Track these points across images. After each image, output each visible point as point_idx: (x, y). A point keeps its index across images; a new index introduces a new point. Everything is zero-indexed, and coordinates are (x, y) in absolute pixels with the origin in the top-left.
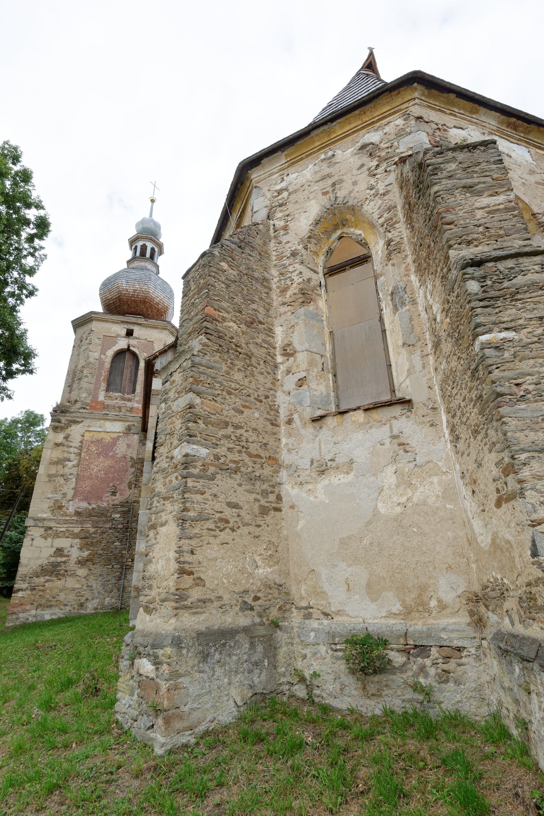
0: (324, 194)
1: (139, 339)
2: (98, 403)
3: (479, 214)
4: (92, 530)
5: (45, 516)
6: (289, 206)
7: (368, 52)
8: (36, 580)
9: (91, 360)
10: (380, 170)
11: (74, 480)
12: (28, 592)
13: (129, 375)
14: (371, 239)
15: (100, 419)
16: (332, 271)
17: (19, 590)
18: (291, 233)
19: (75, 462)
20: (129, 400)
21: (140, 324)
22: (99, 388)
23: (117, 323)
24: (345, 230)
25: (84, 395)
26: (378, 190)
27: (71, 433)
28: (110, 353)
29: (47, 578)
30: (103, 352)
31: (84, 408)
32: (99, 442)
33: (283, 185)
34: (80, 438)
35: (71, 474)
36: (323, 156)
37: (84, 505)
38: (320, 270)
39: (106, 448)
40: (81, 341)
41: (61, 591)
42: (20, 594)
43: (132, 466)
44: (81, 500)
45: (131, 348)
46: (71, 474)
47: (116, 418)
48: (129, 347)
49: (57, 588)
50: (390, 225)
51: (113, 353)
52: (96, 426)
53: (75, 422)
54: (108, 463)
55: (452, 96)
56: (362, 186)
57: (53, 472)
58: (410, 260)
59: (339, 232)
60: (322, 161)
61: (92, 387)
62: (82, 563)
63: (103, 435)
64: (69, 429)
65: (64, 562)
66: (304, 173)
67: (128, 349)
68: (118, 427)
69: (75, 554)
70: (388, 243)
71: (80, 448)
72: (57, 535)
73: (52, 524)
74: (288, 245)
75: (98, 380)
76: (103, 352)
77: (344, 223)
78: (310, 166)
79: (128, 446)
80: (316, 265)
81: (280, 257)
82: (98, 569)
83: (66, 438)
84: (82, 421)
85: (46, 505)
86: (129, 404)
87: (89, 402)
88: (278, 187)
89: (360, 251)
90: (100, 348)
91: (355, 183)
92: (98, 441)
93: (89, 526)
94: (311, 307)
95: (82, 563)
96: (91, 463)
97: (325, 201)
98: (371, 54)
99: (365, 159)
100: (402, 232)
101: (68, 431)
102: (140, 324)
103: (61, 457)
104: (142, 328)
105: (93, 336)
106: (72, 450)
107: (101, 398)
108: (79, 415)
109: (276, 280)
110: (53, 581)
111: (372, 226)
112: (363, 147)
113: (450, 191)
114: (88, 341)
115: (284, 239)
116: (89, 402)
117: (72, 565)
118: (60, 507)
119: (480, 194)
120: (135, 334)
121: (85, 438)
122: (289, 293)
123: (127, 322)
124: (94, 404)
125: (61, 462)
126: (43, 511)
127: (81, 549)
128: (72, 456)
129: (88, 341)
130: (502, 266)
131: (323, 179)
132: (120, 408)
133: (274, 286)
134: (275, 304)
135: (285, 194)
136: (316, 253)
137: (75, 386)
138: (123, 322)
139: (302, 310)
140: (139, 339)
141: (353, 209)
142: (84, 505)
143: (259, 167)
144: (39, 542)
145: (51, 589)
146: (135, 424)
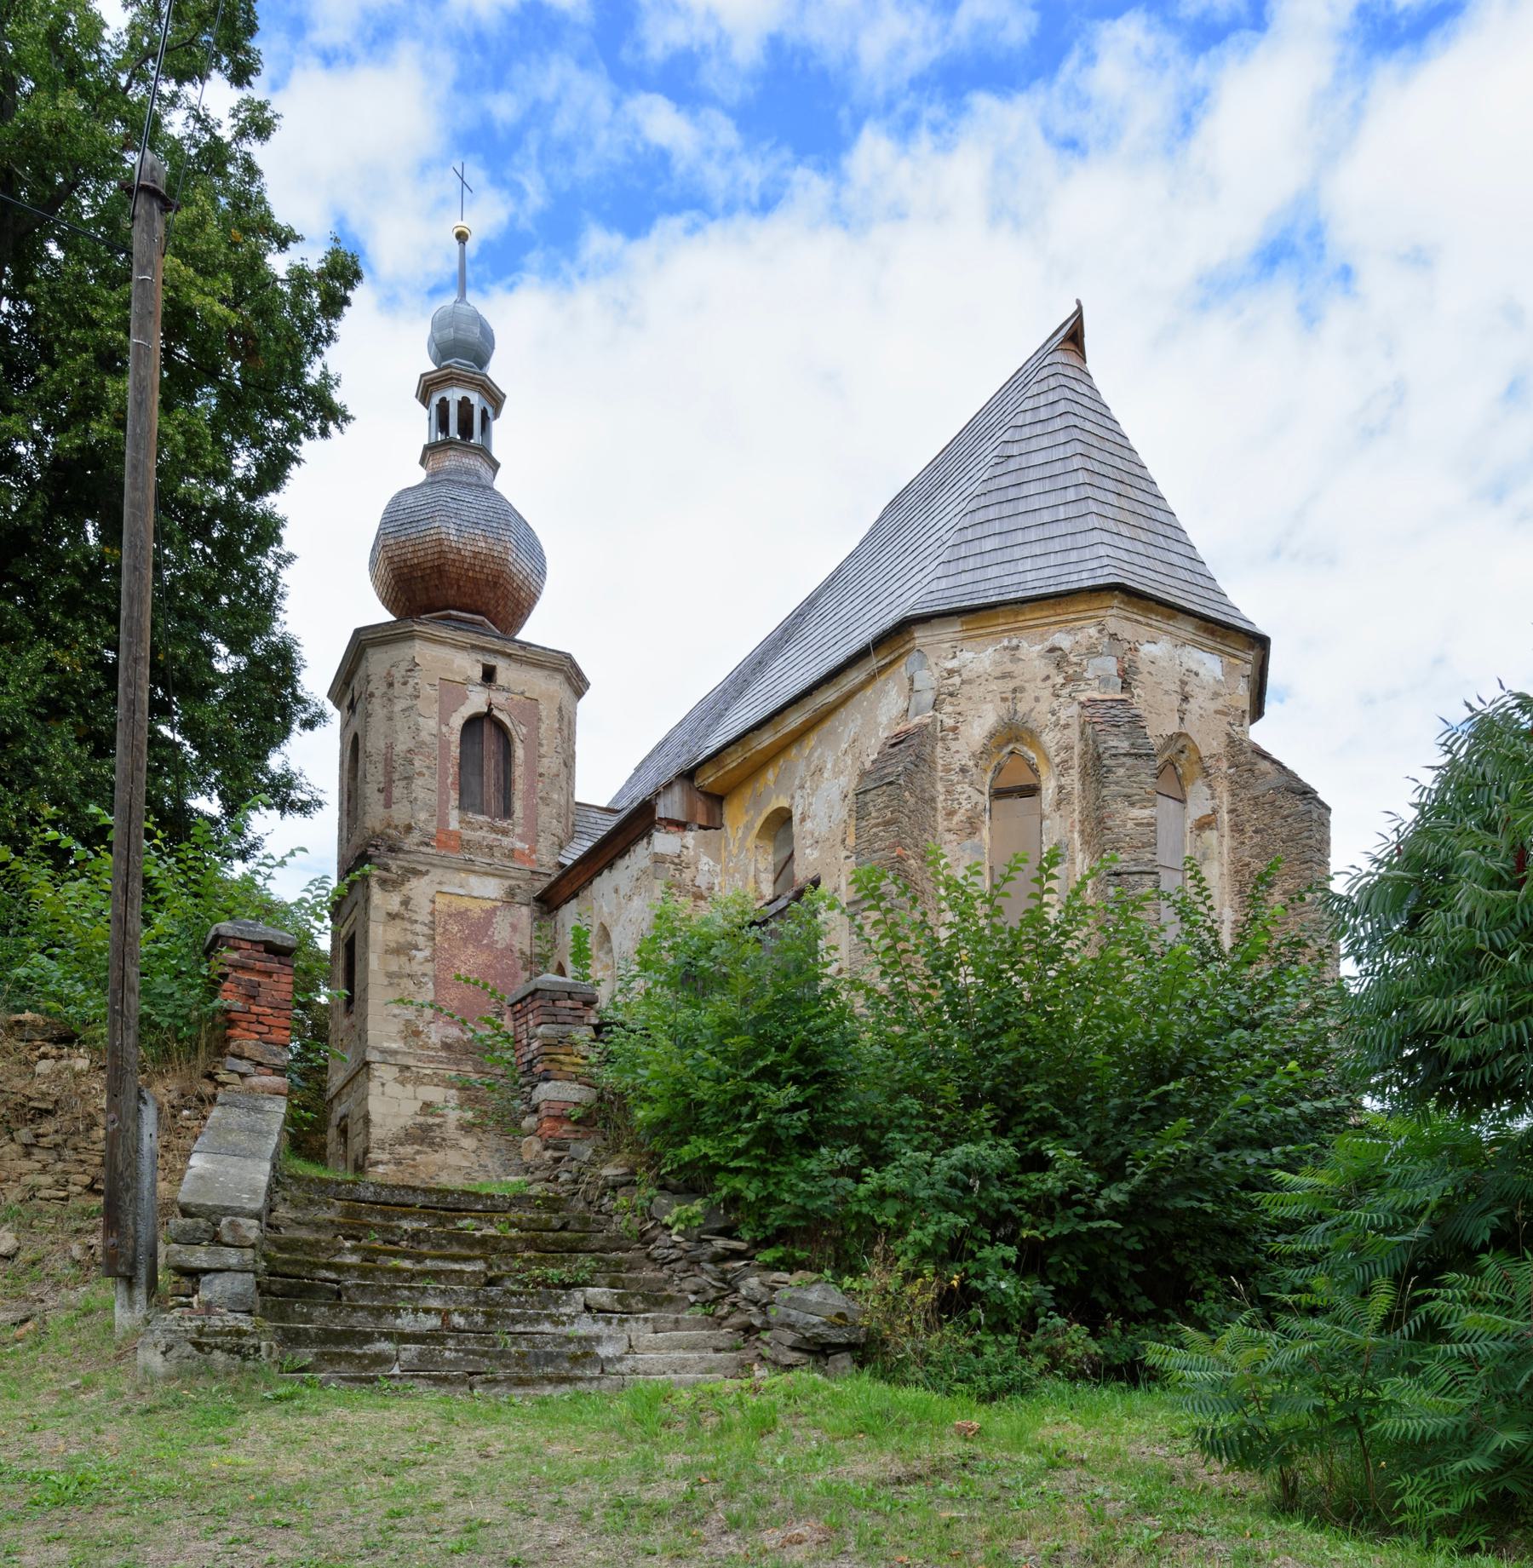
0: (1004, 700)
1: (508, 690)
2: (450, 834)
3: (1130, 824)
4: (474, 1076)
5: (394, 1046)
7: (1075, 307)
8: (401, 1149)
9: (424, 736)
10: (1065, 692)
11: (430, 985)
12: (392, 1167)
13: (493, 775)
14: (1043, 770)
15: (458, 870)
16: (999, 794)
17: (377, 1163)
19: (427, 953)
20: (505, 833)
21: (509, 656)
22: (448, 802)
23: (463, 648)
24: (1018, 746)
25: (423, 816)
26: (1058, 719)
27: (411, 894)
28: (457, 721)
29: (416, 1147)
30: (444, 720)
31: (427, 845)
32: (461, 915)
34: (428, 907)
35: (424, 975)
36: (1006, 643)
37: (454, 1032)
38: (986, 789)
39: (477, 929)
40: (391, 685)
41: (441, 1169)
42: (381, 1169)
43: (525, 969)
44: (448, 1023)
45: (496, 712)
46: (424, 975)
47: (488, 869)
48: (490, 710)
49: (435, 1164)
50: (1064, 767)
51: (462, 722)
52: (455, 882)
53: (417, 873)
54: (483, 958)
55: (1152, 604)
56: (1043, 707)
57: (395, 968)
58: (1076, 815)
59: (1011, 747)
60: (1006, 648)
61: (434, 798)
62: (467, 1128)
63: (466, 903)
64: (408, 886)
65: (439, 1126)
66: (979, 657)
68: (490, 888)
69: (453, 1116)
70: (1061, 788)
71: (432, 925)
72: (419, 1080)
73: (411, 1062)
74: (958, 756)
75: (442, 782)
76: (444, 720)
78: (990, 650)
79: (514, 927)
80: (984, 784)
82: (492, 1141)
83: (406, 903)
84: (427, 872)
85: (394, 1028)
86: (506, 841)
87: (434, 831)
88: (950, 665)
89: (1027, 779)
90: (436, 707)
92: (460, 913)
93: (469, 1068)
94: (976, 839)
95: (467, 1128)
96: (455, 956)
97: (1003, 709)
98: (1078, 316)
99: (1052, 671)
100: (1073, 780)
101: (405, 889)
102: (509, 656)
103: (402, 940)
104: (514, 665)
105: (418, 678)
106: (418, 928)
107: (454, 825)
108: (422, 858)
109: (942, 798)
111: (1048, 759)
112: (1052, 650)
113: (1114, 797)
114: (409, 689)
115: (954, 746)
116: (434, 831)
117: (451, 1130)
118: (417, 1034)
119: (1132, 804)
121: (437, 906)
122: (956, 819)
123: (483, 649)
124: (443, 837)
125: (402, 950)
126: (389, 1038)
127: (461, 1106)
128: (421, 941)
129: (409, 689)
130: (1131, 878)
132: (491, 848)
133: (940, 806)
134: (940, 828)
135: (956, 680)
136: (985, 771)
137: (398, 791)
138: (474, 647)
140: (508, 690)
141: (1031, 732)
142: (454, 1032)
143: (927, 626)
144: (393, 1089)
145: (426, 1165)
146: (522, 884)
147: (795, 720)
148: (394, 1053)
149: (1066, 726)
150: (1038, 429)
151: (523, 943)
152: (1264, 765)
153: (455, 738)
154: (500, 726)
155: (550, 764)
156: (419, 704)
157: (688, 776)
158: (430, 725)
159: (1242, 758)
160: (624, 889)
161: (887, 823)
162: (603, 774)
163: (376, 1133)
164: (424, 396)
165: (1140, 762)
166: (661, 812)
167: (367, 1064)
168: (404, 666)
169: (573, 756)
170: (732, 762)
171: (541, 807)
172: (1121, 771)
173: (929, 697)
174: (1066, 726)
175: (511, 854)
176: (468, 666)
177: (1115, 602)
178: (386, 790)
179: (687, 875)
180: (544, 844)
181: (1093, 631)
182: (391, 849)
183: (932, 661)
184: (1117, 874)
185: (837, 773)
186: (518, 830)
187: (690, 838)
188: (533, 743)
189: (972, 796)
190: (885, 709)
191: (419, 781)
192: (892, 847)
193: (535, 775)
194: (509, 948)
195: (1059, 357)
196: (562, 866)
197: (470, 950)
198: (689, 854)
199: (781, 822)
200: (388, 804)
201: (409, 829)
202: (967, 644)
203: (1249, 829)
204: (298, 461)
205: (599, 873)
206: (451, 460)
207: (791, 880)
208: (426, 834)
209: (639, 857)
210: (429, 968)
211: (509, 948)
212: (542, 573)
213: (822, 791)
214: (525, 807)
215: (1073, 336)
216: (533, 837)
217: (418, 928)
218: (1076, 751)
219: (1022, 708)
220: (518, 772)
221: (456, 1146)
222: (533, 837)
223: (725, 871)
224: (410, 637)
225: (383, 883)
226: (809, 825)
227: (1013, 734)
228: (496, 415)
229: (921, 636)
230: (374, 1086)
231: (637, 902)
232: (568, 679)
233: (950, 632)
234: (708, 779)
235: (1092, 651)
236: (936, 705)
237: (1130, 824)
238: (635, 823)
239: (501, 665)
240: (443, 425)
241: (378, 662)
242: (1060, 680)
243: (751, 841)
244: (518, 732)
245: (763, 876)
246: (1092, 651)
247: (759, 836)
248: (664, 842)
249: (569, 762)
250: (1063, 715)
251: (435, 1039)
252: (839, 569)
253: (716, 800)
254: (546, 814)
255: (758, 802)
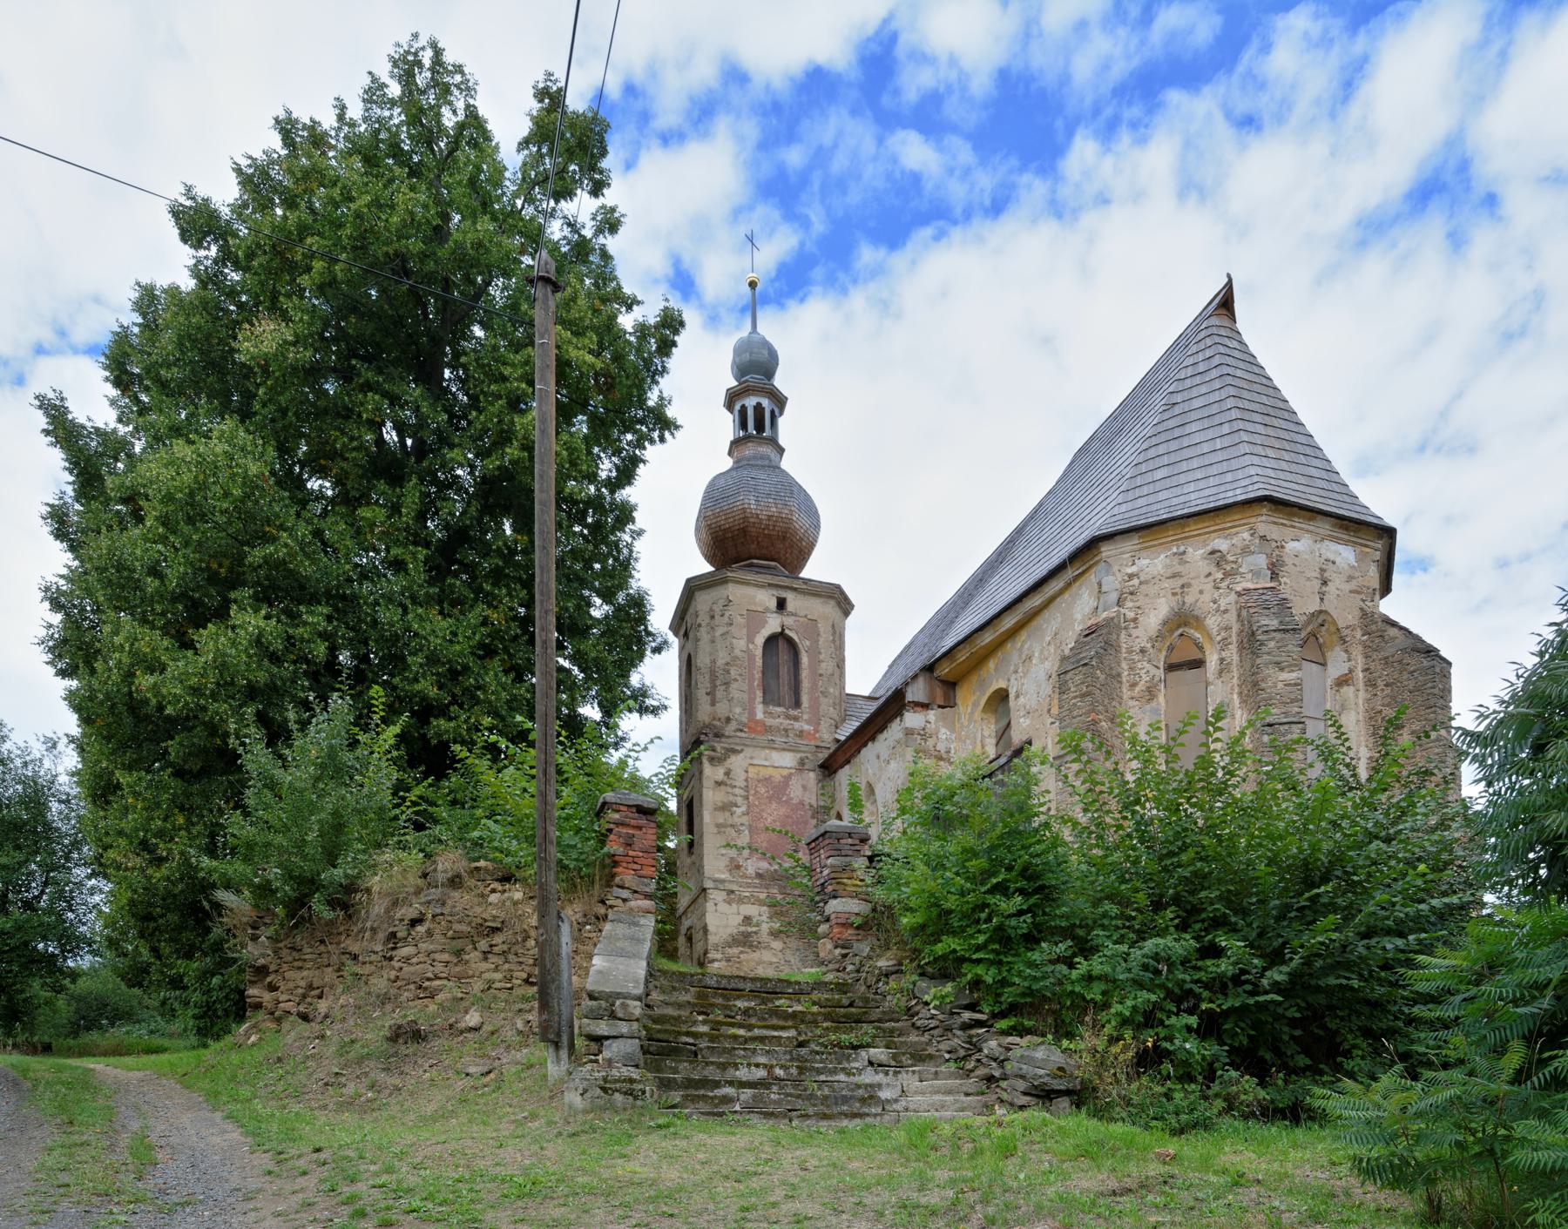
0: (1174, 594)
2: (757, 722)
3: (1280, 685)
4: (780, 897)
6: (1141, 597)
8: (728, 950)
9: (737, 652)
10: (1223, 585)
13: (786, 677)
16: (1171, 668)
18: (1141, 628)
19: (744, 809)
20: (796, 719)
28: (760, 640)
32: (767, 780)
33: (1133, 569)
34: (743, 776)
37: (764, 865)
38: (1161, 665)
39: (778, 790)
40: (713, 617)
41: (758, 964)
42: (716, 965)
50: (1225, 644)
54: (783, 811)
56: (1207, 597)
58: (1235, 681)
61: (745, 696)
62: (775, 934)
63: (770, 771)
66: (1153, 563)
67: (782, 634)
68: (787, 760)
70: (1222, 660)
72: (741, 901)
73: (734, 888)
76: (751, 640)
77: (1186, 624)
79: (804, 788)
81: (1130, 652)
82: (793, 943)
83: (727, 773)
85: (723, 863)
86: (797, 725)
88: (1130, 570)
89: (1196, 655)
90: (744, 631)
91: (1201, 592)
94: (1154, 704)
95: (775, 934)
97: (1173, 601)
98: (1229, 286)
99: (1213, 569)
100: (1232, 654)
106: (737, 791)
107: (760, 715)
110: (1556, 1057)
112: (1213, 553)
114: (726, 619)
115: (1135, 633)
118: (738, 867)
119: (1282, 669)
120: (790, 606)
122: (1137, 689)
125: (726, 807)
128: (739, 800)
129: (726, 619)
131: (1174, 576)
132: (786, 730)
135: (1136, 582)
137: (720, 694)
138: (770, 585)
139: (1148, 707)
141: (1197, 618)
142: (764, 865)
144: (723, 907)
147: (1009, 622)
148: (723, 881)
149: (1226, 611)
150: (1198, 380)
151: (811, 798)
152: (1393, 632)
153: (759, 652)
154: (790, 641)
155: (827, 666)
156: (732, 629)
157: (929, 669)
158: (741, 644)
159: (1374, 627)
160: (885, 754)
161: (1083, 695)
162: (866, 668)
163: (712, 939)
164: (729, 406)
165: (1288, 635)
166: (909, 697)
167: (704, 890)
168: (722, 602)
169: (843, 660)
170: (962, 656)
171: (822, 699)
172: (1272, 644)
173: (1114, 597)
174: (1226, 611)
175: (801, 734)
176: (767, 599)
177: (1264, 511)
178: (711, 693)
179: (930, 743)
180: (825, 726)
181: (1246, 535)
182: (716, 735)
183: (1116, 568)
184: (1270, 725)
185: (1043, 660)
186: (806, 717)
187: (932, 715)
188: (815, 652)
189: (1150, 670)
190: (1080, 607)
191: (734, 685)
192: (1088, 713)
193: (816, 675)
194: (802, 803)
195: (1215, 321)
196: (838, 741)
197: (774, 805)
198: (931, 727)
199: (1001, 698)
200: (713, 703)
201: (728, 720)
202: (1143, 553)
203: (1381, 684)
204: (644, 462)
205: (865, 745)
206: (749, 450)
207: (1009, 743)
208: (740, 723)
209: (894, 731)
210: (745, 820)
211: (802, 803)
212: (817, 527)
213: (1031, 674)
214: (811, 699)
215: (1225, 303)
216: (816, 721)
217: (737, 791)
218: (1235, 630)
219: (1189, 599)
220: (805, 674)
221: (768, 947)
222: (816, 721)
223: (959, 739)
224: (724, 581)
225: (711, 759)
226: (1022, 700)
227: (1182, 620)
228: (781, 413)
229: (1106, 550)
230: (710, 906)
231: (893, 765)
232: (839, 604)
233: (1129, 545)
234: (944, 670)
235: (1246, 551)
236: (1119, 603)
237: (1280, 685)
238: (892, 706)
239: (790, 597)
240: (743, 424)
241: (703, 601)
242: (1220, 575)
243: (978, 714)
244: (804, 645)
245: (988, 741)
246: (1246, 551)
247: (984, 710)
248: (912, 719)
249: (840, 665)
250: (1223, 603)
251: (751, 871)
252: (1041, 504)
253: (951, 685)
254: (825, 704)
255: (982, 684)
